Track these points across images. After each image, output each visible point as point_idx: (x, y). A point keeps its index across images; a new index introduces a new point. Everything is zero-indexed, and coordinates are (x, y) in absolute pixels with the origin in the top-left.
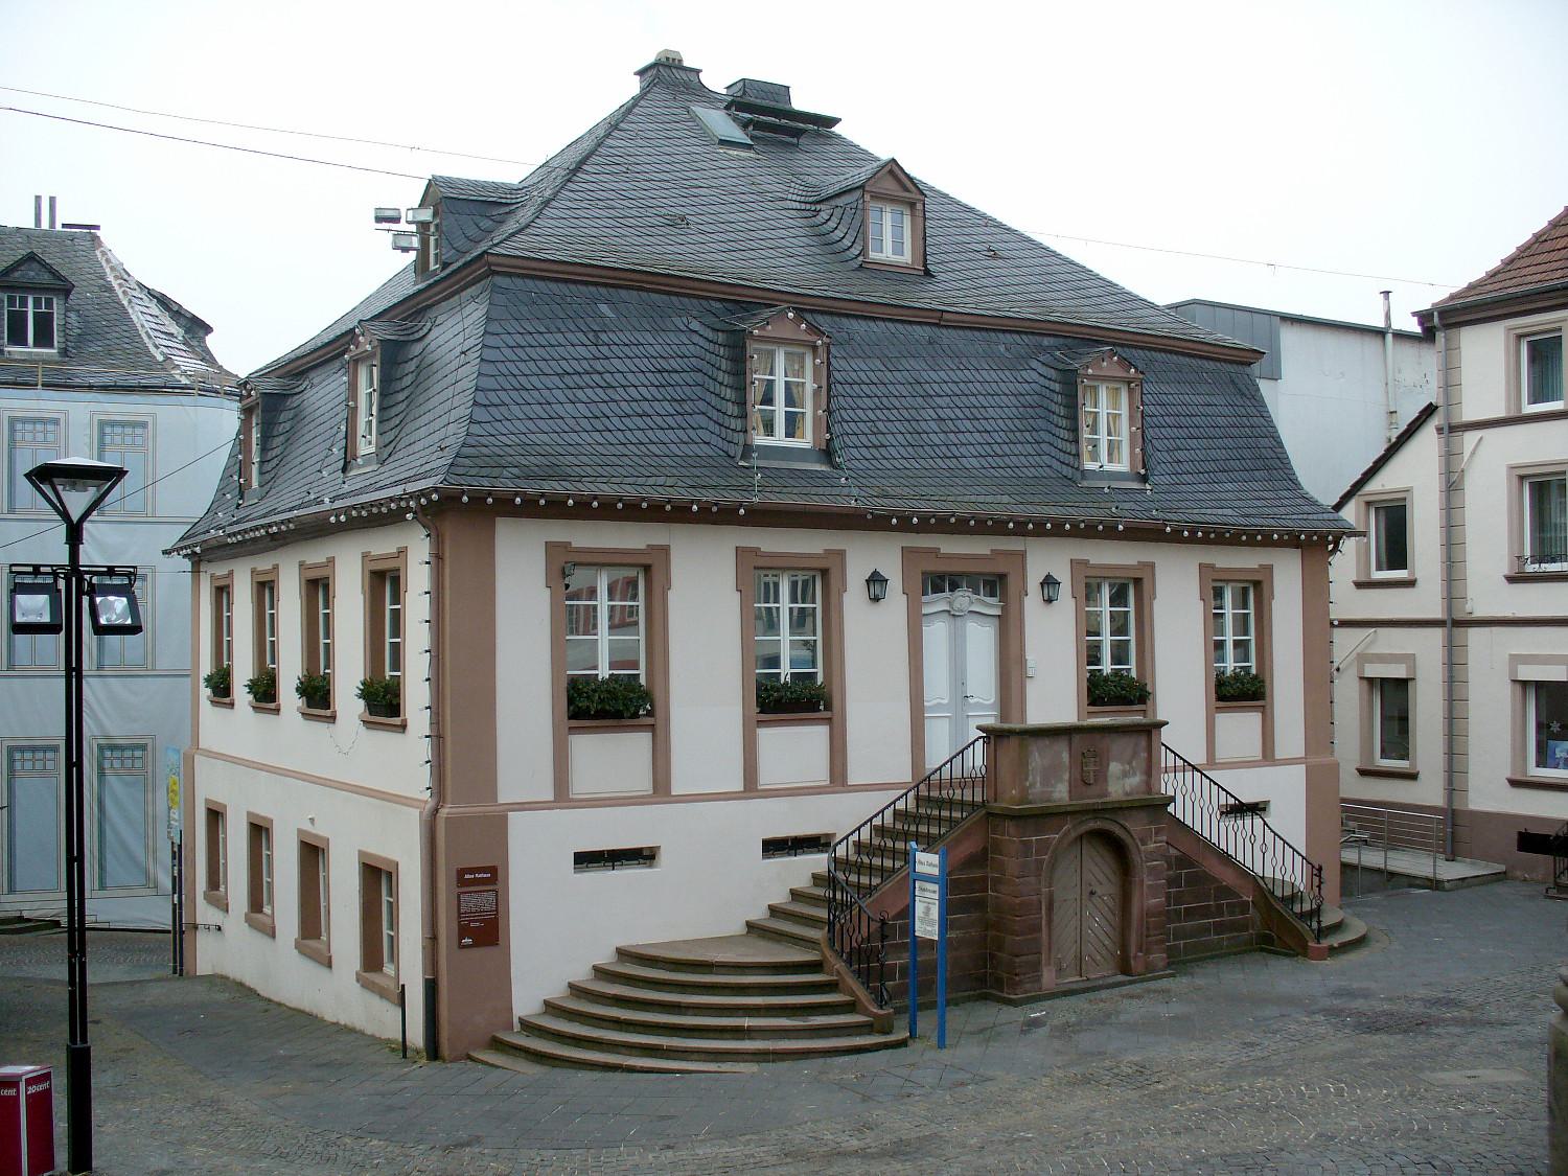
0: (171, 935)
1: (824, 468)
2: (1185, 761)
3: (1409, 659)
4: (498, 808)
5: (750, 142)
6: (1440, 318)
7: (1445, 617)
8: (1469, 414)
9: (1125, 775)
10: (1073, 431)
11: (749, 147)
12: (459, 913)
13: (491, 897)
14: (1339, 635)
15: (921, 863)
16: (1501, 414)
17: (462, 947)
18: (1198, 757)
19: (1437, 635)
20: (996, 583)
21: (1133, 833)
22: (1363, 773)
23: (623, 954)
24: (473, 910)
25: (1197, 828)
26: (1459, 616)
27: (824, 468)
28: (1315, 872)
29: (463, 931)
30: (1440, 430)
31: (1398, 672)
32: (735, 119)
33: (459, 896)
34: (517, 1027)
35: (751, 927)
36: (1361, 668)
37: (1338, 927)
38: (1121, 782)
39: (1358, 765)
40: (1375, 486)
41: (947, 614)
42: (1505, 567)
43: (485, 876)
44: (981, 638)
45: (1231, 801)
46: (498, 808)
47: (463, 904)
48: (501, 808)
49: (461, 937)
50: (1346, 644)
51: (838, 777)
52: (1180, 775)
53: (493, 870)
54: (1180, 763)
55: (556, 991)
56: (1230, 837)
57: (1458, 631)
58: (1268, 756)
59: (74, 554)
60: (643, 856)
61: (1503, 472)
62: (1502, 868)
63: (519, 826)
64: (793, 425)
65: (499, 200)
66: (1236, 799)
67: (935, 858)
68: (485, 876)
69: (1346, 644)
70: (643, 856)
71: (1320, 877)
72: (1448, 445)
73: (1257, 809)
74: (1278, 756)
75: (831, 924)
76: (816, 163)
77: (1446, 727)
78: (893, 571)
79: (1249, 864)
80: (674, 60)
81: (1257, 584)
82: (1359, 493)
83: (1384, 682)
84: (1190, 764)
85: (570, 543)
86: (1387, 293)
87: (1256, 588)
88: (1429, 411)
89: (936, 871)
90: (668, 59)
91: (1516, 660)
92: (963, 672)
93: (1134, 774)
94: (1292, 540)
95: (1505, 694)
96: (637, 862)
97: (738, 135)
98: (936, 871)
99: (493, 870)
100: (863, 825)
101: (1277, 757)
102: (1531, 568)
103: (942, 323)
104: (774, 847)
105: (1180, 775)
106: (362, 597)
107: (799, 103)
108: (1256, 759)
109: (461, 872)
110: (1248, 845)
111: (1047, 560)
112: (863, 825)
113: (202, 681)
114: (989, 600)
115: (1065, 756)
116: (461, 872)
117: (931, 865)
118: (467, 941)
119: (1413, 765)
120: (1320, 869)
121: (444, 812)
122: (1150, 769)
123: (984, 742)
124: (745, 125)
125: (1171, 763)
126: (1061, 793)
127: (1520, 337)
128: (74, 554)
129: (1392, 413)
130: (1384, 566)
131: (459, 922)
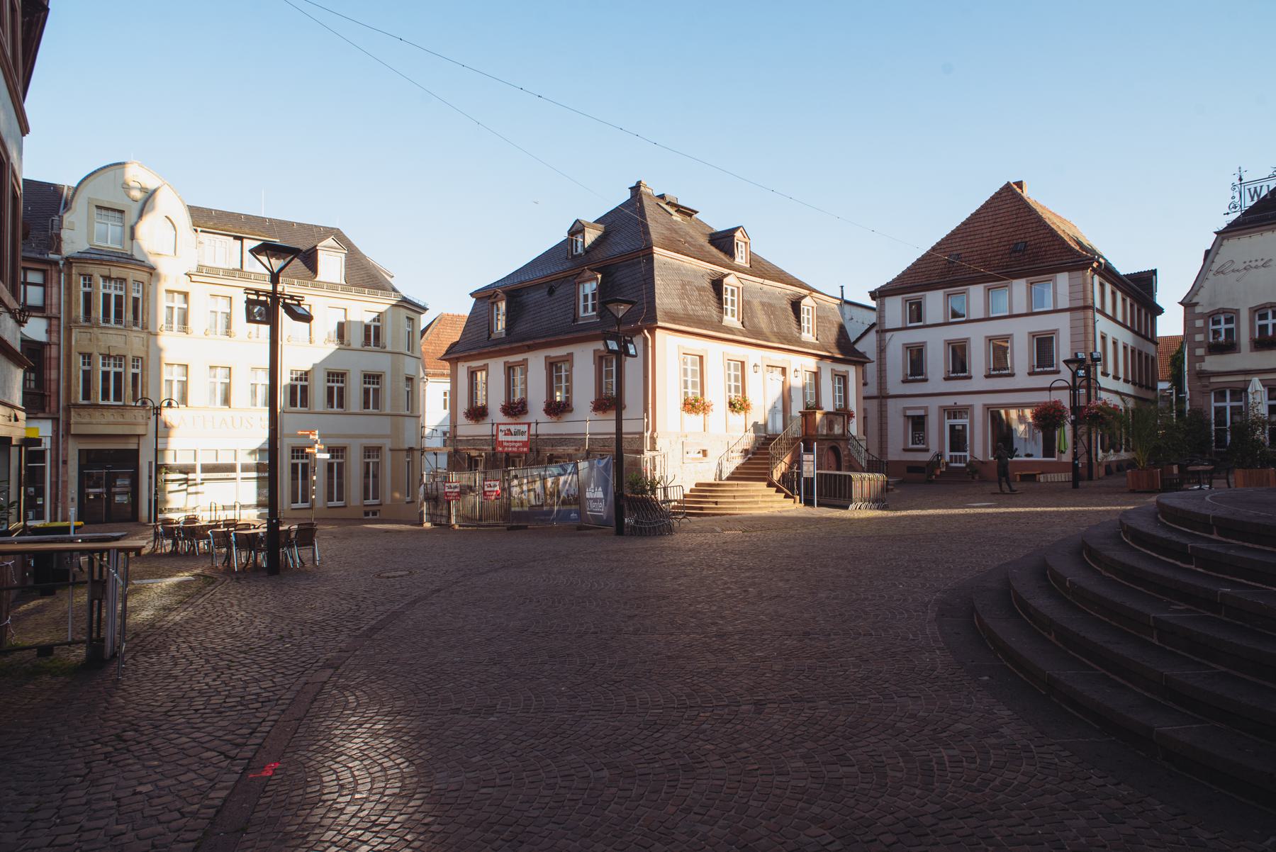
0: (21, 254)
3: (926, 408)
8: (888, 326)
16: (900, 326)
19: (875, 402)
26: (883, 395)
30: (877, 332)
31: (921, 413)
42: (901, 378)
57: (883, 400)
61: (983, 339)
62: (901, 479)
72: (880, 337)
83: (913, 417)
86: (842, 287)
88: (873, 325)
91: (906, 409)
95: (901, 420)
102: (993, 373)
106: (545, 372)
108: (73, 398)
113: (855, 415)
127: (906, 301)
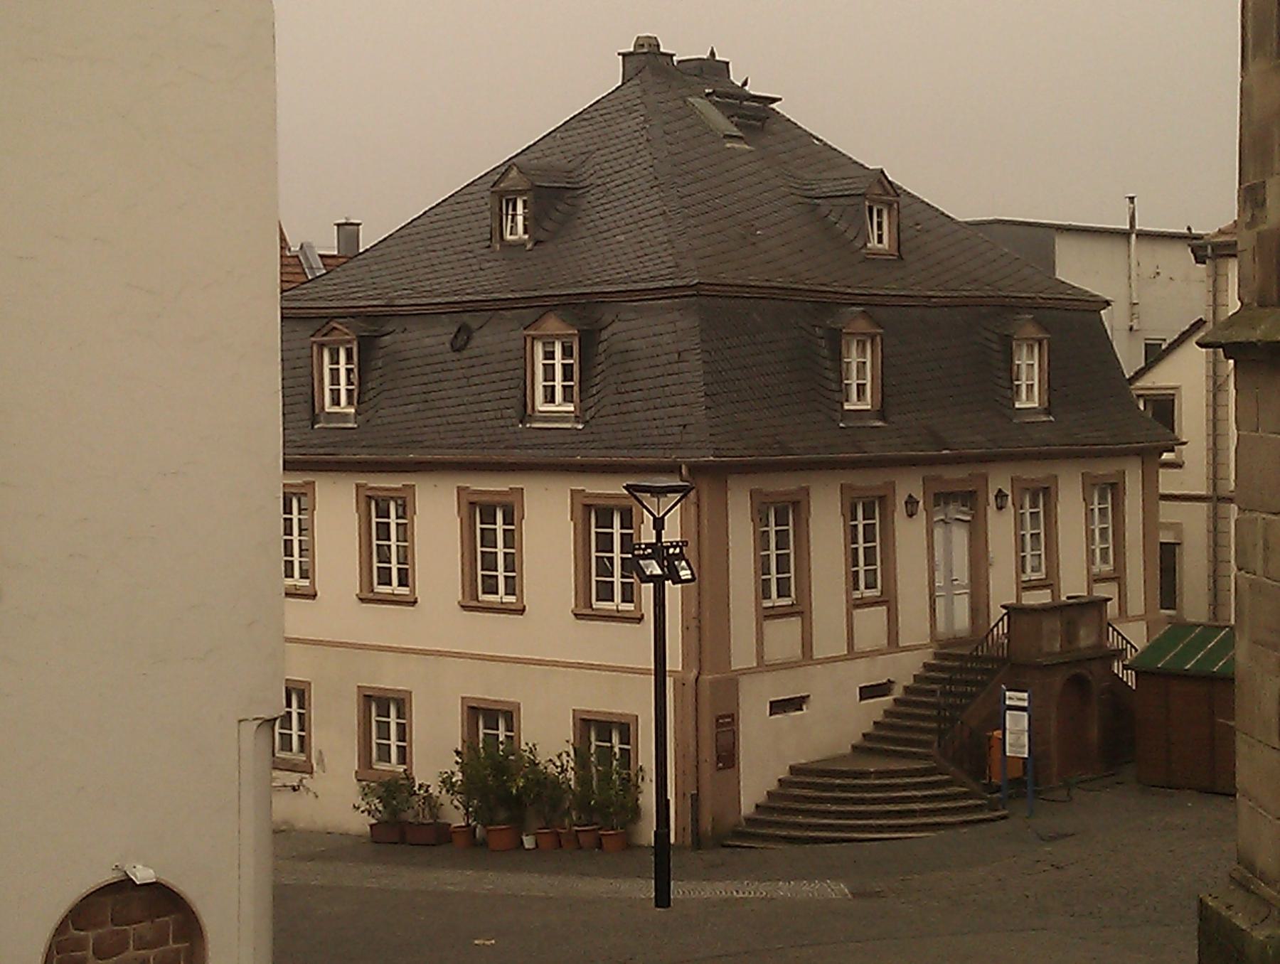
5: (740, 134)
6: (1213, 250)
7: (1210, 493)
20: (970, 498)
23: (794, 770)
38: (1086, 638)
41: (941, 523)
44: (960, 536)
46: (730, 674)
53: (732, 716)
55: (761, 798)
57: (1222, 505)
59: (659, 536)
65: (568, 186)
74: (1130, 613)
75: (940, 733)
78: (919, 496)
81: (1113, 486)
87: (1115, 489)
92: (951, 564)
94: (1138, 453)
97: (735, 131)
111: (1000, 480)
114: (964, 509)
115: (1059, 624)
119: (413, 591)
128: (659, 536)
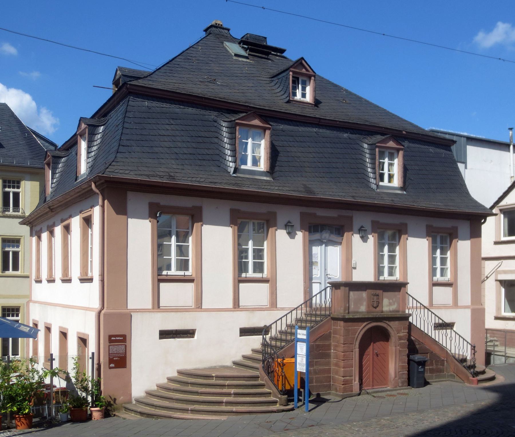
1: (268, 179)
2: (421, 304)
4: (127, 311)
9: (390, 304)
10: (373, 169)
11: (247, 58)
12: (109, 354)
13: (123, 347)
14: (487, 263)
15: (300, 334)
17: (110, 368)
18: (426, 303)
21: (393, 328)
22: (497, 318)
23: (180, 373)
24: (115, 352)
25: (422, 329)
27: (268, 179)
28: (472, 348)
29: (111, 361)
32: (243, 47)
33: (109, 346)
34: (134, 402)
35: (235, 363)
36: (496, 275)
37: (483, 372)
39: (495, 315)
40: (503, 203)
43: (120, 338)
45: (441, 321)
46: (127, 311)
47: (111, 350)
48: (128, 311)
49: (110, 364)
50: (489, 267)
51: (273, 304)
52: (419, 310)
53: (124, 336)
54: (419, 305)
56: (439, 336)
58: (456, 304)
60: (189, 333)
63: (137, 320)
64: (256, 162)
66: (443, 321)
67: (304, 332)
68: (120, 338)
69: (489, 267)
70: (189, 333)
71: (474, 350)
73: (449, 326)
75: (263, 361)
76: (274, 66)
77: (504, 143)
79: (444, 345)
80: (219, 24)
82: (498, 206)
84: (423, 305)
85: (159, 203)
89: (305, 337)
90: (216, 24)
93: (394, 304)
96: (186, 335)
97: (243, 52)
98: (305, 337)
99: (124, 336)
100: (278, 320)
101: (459, 305)
103: (320, 123)
104: (245, 332)
105: (419, 310)
107: (270, 43)
109: (110, 337)
110: (444, 337)
112: (278, 320)
116: (110, 337)
117: (303, 334)
118: (112, 365)
120: (474, 347)
121: (103, 312)
122: (404, 302)
123: (330, 289)
124: (246, 50)
125: (415, 305)
126: (363, 308)
129: (512, 177)
130: (507, 235)
131: (109, 357)
